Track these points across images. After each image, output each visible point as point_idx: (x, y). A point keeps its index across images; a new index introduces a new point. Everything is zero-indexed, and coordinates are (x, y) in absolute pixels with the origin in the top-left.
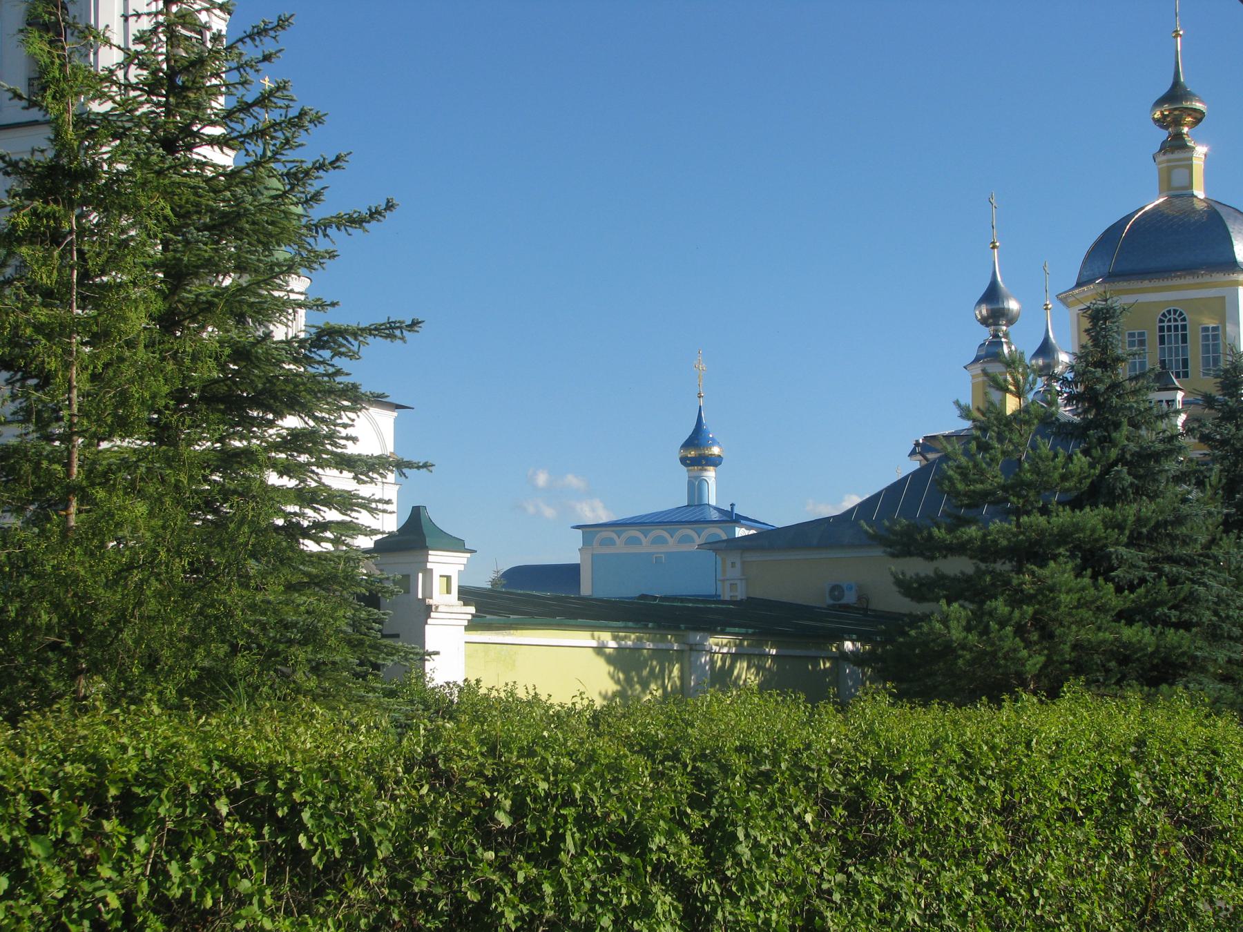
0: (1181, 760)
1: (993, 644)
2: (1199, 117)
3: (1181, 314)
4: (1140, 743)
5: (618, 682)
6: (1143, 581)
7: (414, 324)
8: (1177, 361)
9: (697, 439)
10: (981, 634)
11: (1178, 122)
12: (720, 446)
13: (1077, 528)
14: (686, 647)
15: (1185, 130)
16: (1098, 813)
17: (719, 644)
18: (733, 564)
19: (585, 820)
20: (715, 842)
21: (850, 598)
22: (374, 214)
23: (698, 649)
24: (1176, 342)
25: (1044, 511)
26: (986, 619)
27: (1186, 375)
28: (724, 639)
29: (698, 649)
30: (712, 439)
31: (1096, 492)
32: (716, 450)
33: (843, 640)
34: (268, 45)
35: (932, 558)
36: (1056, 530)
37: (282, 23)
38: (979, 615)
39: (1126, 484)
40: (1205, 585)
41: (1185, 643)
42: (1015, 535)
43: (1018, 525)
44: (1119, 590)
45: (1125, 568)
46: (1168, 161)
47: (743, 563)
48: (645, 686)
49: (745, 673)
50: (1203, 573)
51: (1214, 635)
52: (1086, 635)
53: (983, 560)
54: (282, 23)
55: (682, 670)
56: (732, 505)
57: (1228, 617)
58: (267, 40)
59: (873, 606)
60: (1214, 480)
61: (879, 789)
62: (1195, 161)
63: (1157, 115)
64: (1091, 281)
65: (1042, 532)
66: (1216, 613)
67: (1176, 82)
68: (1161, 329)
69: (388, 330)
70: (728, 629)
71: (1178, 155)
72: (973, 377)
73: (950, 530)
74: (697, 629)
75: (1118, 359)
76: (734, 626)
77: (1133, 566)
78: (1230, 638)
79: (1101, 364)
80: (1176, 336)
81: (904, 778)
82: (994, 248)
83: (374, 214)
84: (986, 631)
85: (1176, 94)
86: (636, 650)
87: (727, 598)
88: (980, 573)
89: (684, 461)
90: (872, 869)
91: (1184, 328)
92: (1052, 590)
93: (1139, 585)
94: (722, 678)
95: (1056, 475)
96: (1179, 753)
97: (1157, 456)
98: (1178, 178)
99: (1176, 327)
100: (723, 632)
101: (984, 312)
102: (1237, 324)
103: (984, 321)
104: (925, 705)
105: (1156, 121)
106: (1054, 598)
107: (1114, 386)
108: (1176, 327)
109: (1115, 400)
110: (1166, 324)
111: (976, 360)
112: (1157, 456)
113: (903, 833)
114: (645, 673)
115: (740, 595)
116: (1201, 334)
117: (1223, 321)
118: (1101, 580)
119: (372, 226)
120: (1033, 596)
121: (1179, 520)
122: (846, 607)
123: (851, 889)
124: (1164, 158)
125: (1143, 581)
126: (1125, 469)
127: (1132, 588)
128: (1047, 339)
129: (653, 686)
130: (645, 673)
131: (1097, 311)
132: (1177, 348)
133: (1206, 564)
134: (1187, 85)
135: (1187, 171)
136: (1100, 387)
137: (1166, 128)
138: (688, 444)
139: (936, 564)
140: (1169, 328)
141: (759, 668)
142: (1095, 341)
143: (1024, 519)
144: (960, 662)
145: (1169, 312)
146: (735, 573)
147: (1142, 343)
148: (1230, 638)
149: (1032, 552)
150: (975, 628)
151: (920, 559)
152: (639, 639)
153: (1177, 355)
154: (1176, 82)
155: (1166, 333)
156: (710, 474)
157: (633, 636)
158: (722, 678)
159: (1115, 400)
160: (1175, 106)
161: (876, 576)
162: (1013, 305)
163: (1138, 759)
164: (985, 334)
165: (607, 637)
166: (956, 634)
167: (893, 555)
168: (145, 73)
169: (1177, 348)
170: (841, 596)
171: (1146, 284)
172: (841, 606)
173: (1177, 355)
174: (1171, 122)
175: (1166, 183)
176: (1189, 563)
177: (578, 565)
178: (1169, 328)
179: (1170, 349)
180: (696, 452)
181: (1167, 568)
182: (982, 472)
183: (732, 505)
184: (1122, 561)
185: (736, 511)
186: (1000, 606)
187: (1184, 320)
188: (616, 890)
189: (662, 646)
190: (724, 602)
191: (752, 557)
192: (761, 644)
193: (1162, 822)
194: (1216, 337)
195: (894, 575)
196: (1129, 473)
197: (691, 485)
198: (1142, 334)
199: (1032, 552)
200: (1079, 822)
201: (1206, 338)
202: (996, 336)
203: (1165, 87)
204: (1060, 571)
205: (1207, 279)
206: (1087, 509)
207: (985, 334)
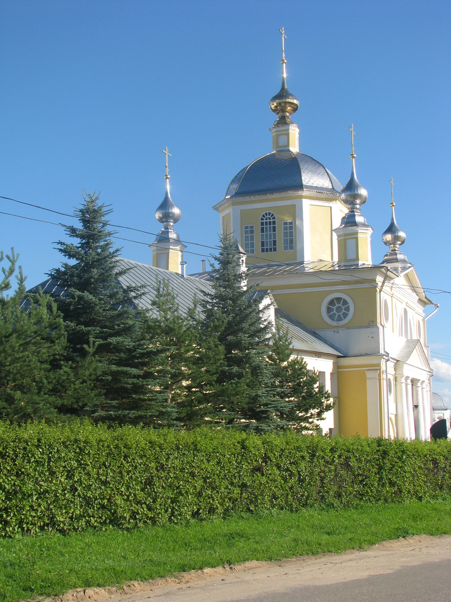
2: (295, 108)
3: (273, 215)
24: (270, 231)
46: (277, 131)
67: (283, 88)
68: (262, 224)
80: (270, 227)
82: (167, 178)
91: (274, 223)
98: (282, 141)
99: (270, 222)
102: (302, 219)
105: (274, 111)
116: (283, 226)
117: (294, 219)
132: (270, 235)
134: (289, 90)
145: (266, 214)
147: (252, 232)
154: (283, 88)
155: (265, 226)
162: (176, 211)
169: (270, 235)
171: (252, 198)
174: (280, 109)
177: (446, 437)
179: (267, 235)
187: (274, 218)
194: (291, 228)
198: (252, 227)
201: (285, 228)
203: (277, 91)
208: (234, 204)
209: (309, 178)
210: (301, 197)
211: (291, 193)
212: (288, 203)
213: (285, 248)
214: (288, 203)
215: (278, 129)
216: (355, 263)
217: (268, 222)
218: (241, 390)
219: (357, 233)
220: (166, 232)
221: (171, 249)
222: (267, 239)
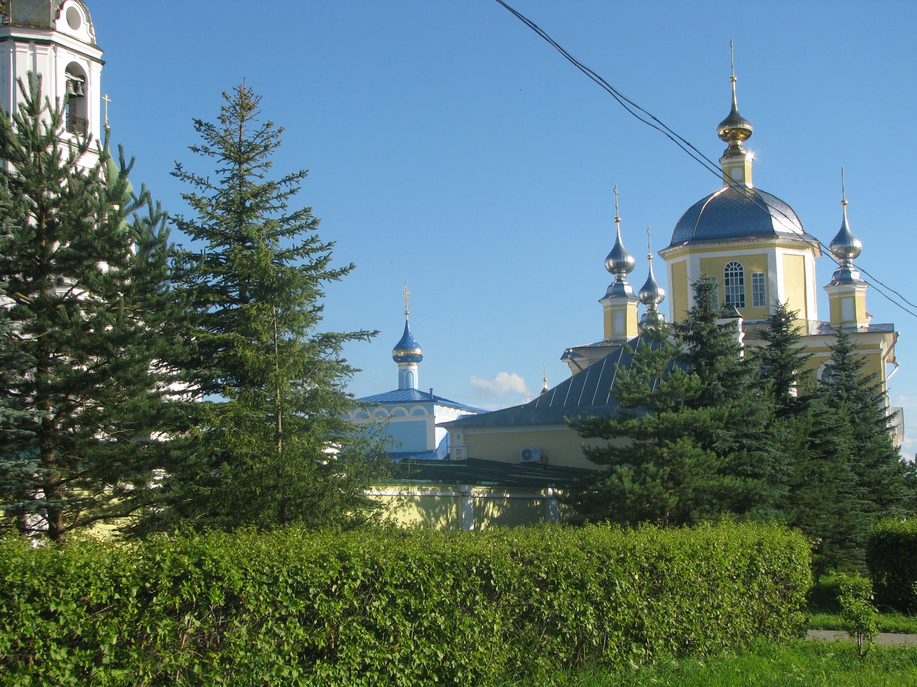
0: (777, 552)
1: (648, 490)
2: (748, 134)
3: (739, 265)
4: (760, 544)
5: (422, 515)
6: (731, 449)
7: (375, 333)
8: (737, 296)
10: (641, 484)
11: (734, 137)
13: (695, 420)
14: (460, 494)
15: (739, 143)
16: (743, 577)
17: (478, 491)
18: (458, 437)
19: (568, 576)
20: (608, 585)
21: (535, 458)
22: (344, 271)
23: (466, 495)
24: (736, 284)
25: (676, 409)
26: (643, 475)
27: (743, 305)
28: (480, 489)
29: (466, 495)
30: (416, 343)
31: (704, 399)
32: (418, 351)
33: (546, 487)
34: (294, 185)
35: (607, 438)
36: (682, 422)
37: (302, 174)
38: (638, 473)
39: (720, 392)
40: (767, 451)
41: (759, 486)
42: (658, 424)
43: (659, 418)
44: (719, 456)
45: (720, 441)
46: (729, 163)
47: (465, 436)
48: (437, 519)
49: (493, 511)
50: (765, 444)
51: (773, 481)
52: (700, 483)
53: (638, 439)
54: (302, 174)
55: (457, 508)
56: (431, 390)
57: (780, 470)
58: (293, 183)
59: (552, 462)
60: (770, 385)
61: (662, 565)
62: (746, 164)
63: (721, 133)
64: (681, 243)
65: (674, 423)
66: (774, 468)
67: (733, 112)
68: (727, 275)
69: (359, 336)
70: (483, 483)
71: (734, 159)
72: (605, 307)
73: (620, 422)
74: (466, 483)
75: (713, 315)
76: (487, 481)
77: (725, 440)
78: (781, 482)
79: (705, 319)
80: (736, 280)
81: (670, 560)
83: (344, 271)
84: (643, 483)
85: (733, 119)
86: (432, 496)
87: (455, 459)
88: (638, 447)
89: (396, 358)
90: (658, 601)
91: (741, 274)
92: (681, 456)
93: (729, 452)
94: (479, 513)
95: (683, 389)
96: (776, 549)
97: (738, 374)
99: (736, 274)
100: (480, 485)
101: (611, 264)
102: (775, 272)
103: (611, 270)
104: (634, 526)
105: (720, 136)
106: (681, 462)
107: (712, 331)
108: (736, 274)
109: (712, 341)
110: (729, 272)
111: (607, 297)
112: (738, 374)
113: (670, 584)
114: (437, 510)
115: (463, 456)
116: (752, 279)
117: (766, 271)
118: (708, 451)
119: (342, 277)
120: (670, 461)
121: (752, 413)
122: (534, 464)
123: (650, 608)
124: (726, 161)
125: (731, 449)
126: (720, 383)
127: (726, 454)
128: (650, 279)
129: (441, 519)
130: (437, 510)
131: (701, 286)
132: (737, 288)
133: (766, 438)
135: (741, 170)
136: (704, 333)
137: (727, 141)
139: (609, 441)
140: (732, 274)
141: (500, 506)
142: (700, 303)
143: (663, 414)
144: (628, 501)
146: (461, 442)
148: (781, 482)
149: (671, 433)
150: (637, 481)
151: (600, 439)
152: (433, 490)
153: (737, 292)
154: (733, 112)
156: (414, 368)
157: (430, 489)
158: (479, 513)
159: (712, 341)
160: (733, 127)
161: (568, 448)
162: (630, 260)
163: (759, 551)
164: (612, 278)
165: (416, 492)
166: (628, 485)
167: (584, 436)
169: (737, 288)
170: (530, 457)
171: (716, 245)
172: (530, 463)
173: (737, 292)
175: (728, 178)
176: (757, 438)
178: (732, 274)
179: (732, 288)
181: (745, 441)
182: (638, 387)
183: (431, 390)
184: (718, 437)
185: (434, 394)
186: (651, 467)
187: (741, 269)
188: (576, 605)
189: (445, 494)
190: (454, 462)
191: (469, 432)
192: (501, 491)
193: (769, 582)
194: (761, 281)
195: (583, 448)
196: (722, 385)
199: (671, 433)
200: (734, 581)
201: (755, 281)
202: (619, 280)
204: (686, 444)
205: (756, 242)
206: (700, 409)
207: (612, 278)
208: (691, 251)
209: (782, 224)
210: (774, 245)
211: (763, 241)
212: (758, 251)
213: (756, 304)
214: (758, 251)
215: (729, 160)
216: (853, 325)
217: (734, 274)
218: (874, 501)
219: (854, 292)
220: (619, 285)
221: (60, 134)
222: (733, 292)
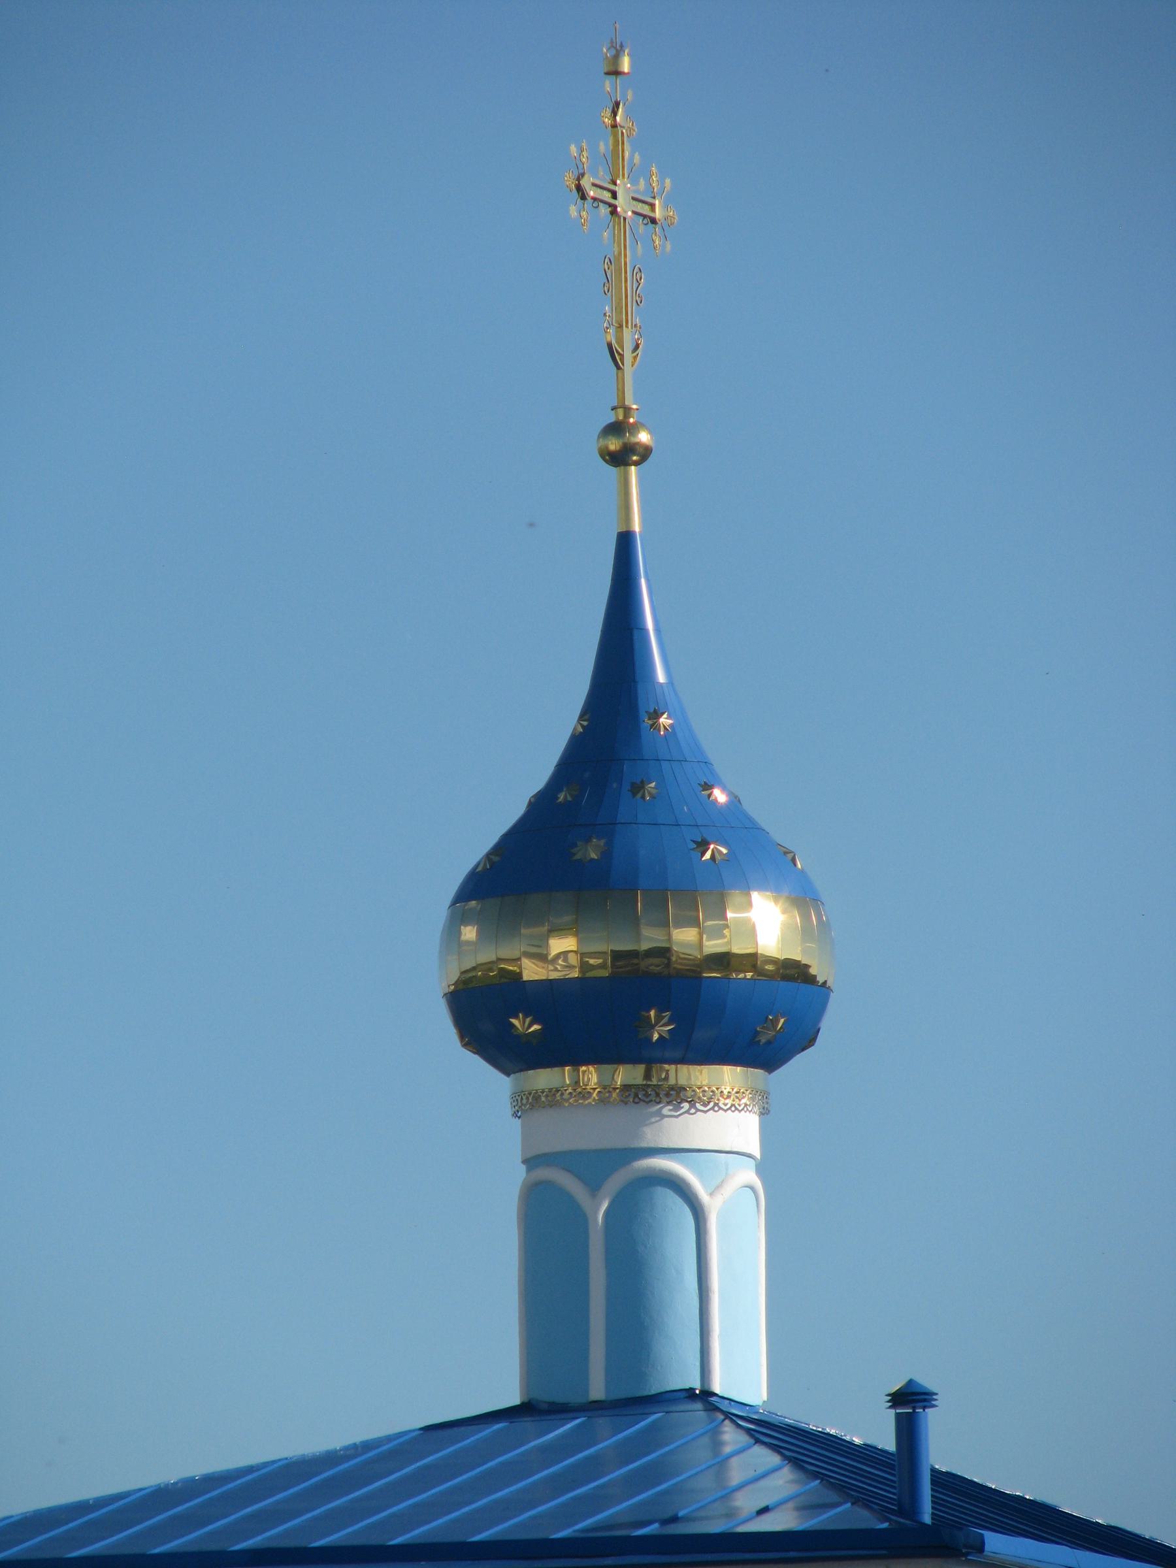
9: (597, 822)
12: (804, 898)
32: (764, 924)
56: (910, 1401)
82: (619, 459)
89: (491, 1017)
138: (530, 868)
156: (720, 1132)
168: (763, 1041)
180: (595, 950)
183: (910, 1401)
185: (947, 1448)
197: (548, 1225)
